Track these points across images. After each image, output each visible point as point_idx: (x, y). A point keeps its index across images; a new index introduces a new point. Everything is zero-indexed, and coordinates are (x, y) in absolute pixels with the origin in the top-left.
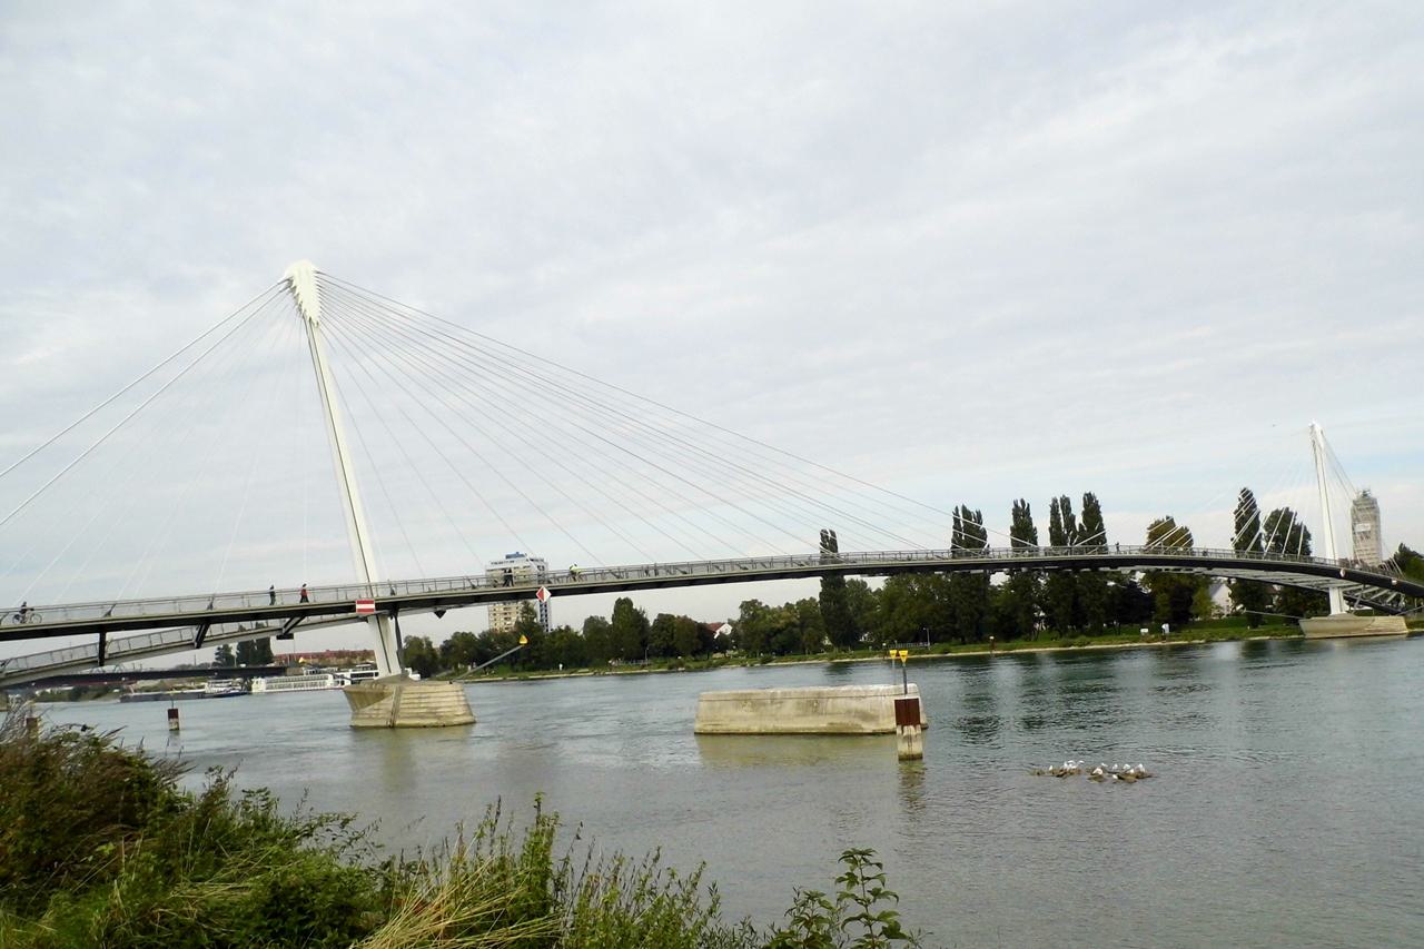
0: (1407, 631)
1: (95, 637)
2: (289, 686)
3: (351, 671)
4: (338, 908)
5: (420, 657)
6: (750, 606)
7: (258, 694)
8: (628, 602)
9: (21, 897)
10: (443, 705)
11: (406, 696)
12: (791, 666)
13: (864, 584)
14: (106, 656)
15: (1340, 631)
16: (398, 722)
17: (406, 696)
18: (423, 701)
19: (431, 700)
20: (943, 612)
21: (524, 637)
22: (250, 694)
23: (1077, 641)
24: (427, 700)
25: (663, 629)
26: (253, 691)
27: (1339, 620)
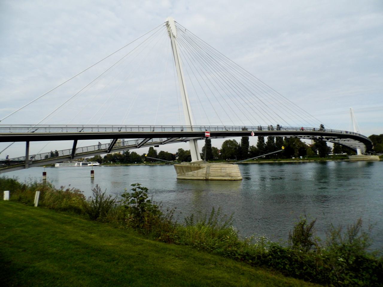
0: (379, 159)
1: (72, 142)
2: (65, 165)
3: (82, 162)
4: (318, 240)
5: (98, 159)
6: (181, 150)
7: (57, 167)
8: (152, 148)
9: (244, 246)
10: (232, 172)
11: (212, 168)
12: (118, 166)
13: (111, 154)
14: (75, 155)
15: (361, 159)
16: (210, 178)
17: (212, 168)
18: (222, 170)
19: (227, 170)
20: (237, 152)
21: (283, 146)
22: (55, 167)
23: (278, 160)
24: (224, 170)
25: (162, 155)
26: (55, 166)
27: (359, 156)
